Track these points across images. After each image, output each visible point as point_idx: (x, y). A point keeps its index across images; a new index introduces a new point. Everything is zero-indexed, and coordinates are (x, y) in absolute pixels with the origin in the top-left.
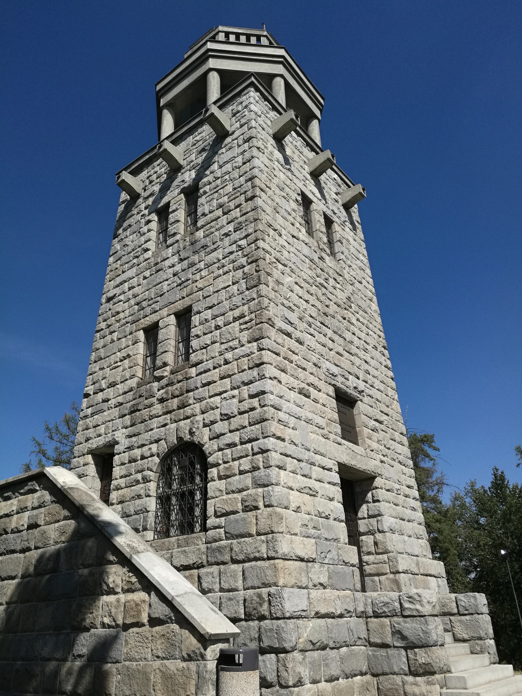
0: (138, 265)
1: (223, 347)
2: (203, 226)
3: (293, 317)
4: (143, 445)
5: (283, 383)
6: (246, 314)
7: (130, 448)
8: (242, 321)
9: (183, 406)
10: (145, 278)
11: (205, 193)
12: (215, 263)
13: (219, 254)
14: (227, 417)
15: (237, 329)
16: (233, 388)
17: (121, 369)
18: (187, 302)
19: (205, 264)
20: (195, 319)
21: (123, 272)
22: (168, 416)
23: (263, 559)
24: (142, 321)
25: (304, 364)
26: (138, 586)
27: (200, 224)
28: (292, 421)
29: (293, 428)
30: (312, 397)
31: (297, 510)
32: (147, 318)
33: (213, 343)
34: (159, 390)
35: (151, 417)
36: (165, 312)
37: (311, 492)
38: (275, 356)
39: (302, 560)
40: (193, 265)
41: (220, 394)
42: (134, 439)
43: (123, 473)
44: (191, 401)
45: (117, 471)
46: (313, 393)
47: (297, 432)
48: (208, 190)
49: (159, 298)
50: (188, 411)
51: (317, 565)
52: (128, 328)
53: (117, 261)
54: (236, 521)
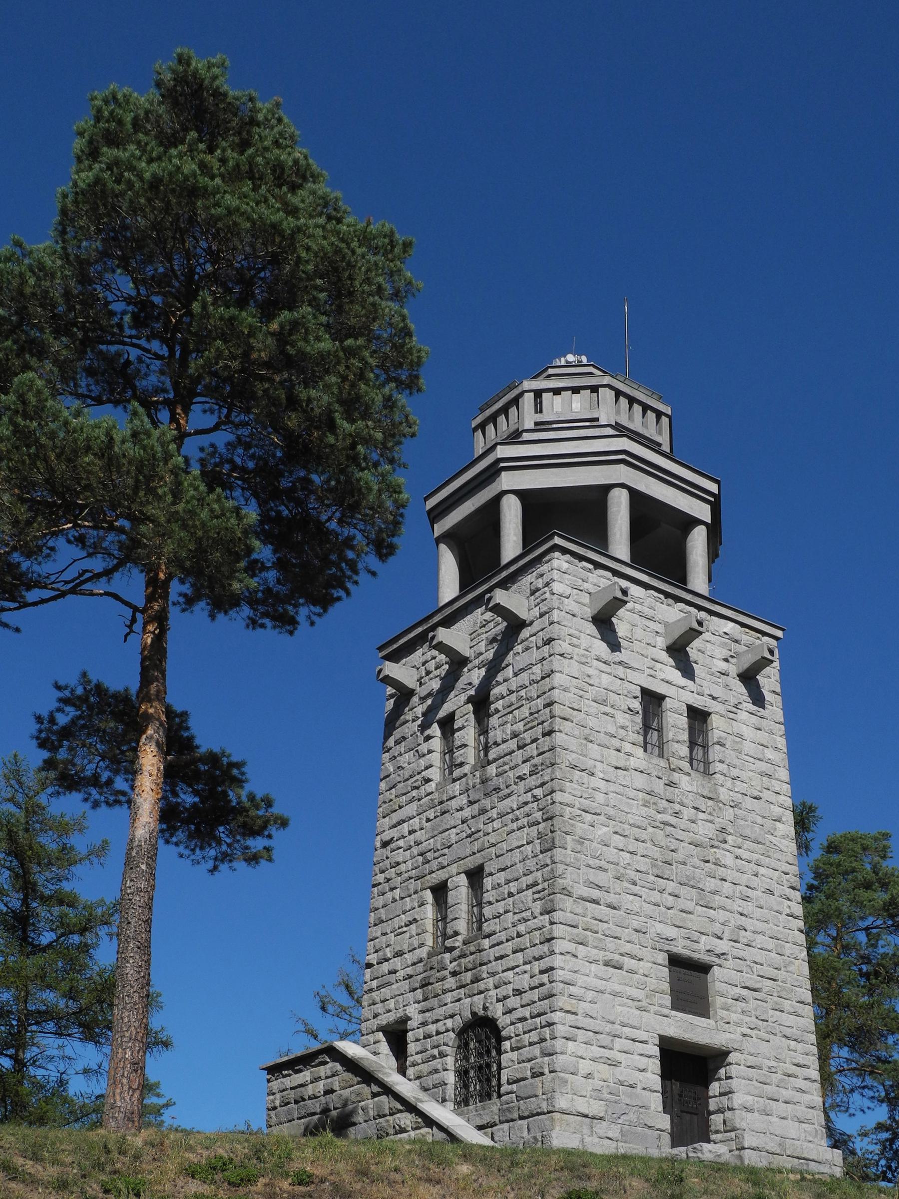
0: (419, 800)
1: (517, 917)
2: (495, 760)
3: (601, 878)
4: (437, 1021)
5: (580, 957)
6: (540, 881)
7: (424, 1024)
8: (535, 889)
9: (476, 980)
10: (428, 820)
11: (497, 711)
12: (508, 813)
13: (512, 802)
14: (518, 992)
15: (530, 899)
16: (525, 963)
17: (407, 935)
18: (477, 860)
19: (498, 814)
20: (488, 882)
21: (400, 807)
22: (462, 991)
23: (544, 1114)
24: (428, 877)
25: (618, 931)
26: (423, 1124)
27: (492, 755)
28: (590, 995)
29: (590, 1002)
30: (625, 968)
31: (588, 1076)
32: (434, 875)
33: (506, 912)
34: (451, 962)
35: (445, 992)
36: (454, 869)
37: (610, 1062)
38: (570, 929)
39: (586, 1116)
40: (483, 811)
41: (513, 968)
42: (427, 1014)
43: (419, 1049)
44: (485, 975)
45: (412, 1048)
46: (628, 963)
47: (596, 1006)
48: (500, 708)
49: (446, 851)
50: (482, 985)
51: (604, 1123)
52: (412, 885)
53: (391, 789)
54: (526, 1086)
